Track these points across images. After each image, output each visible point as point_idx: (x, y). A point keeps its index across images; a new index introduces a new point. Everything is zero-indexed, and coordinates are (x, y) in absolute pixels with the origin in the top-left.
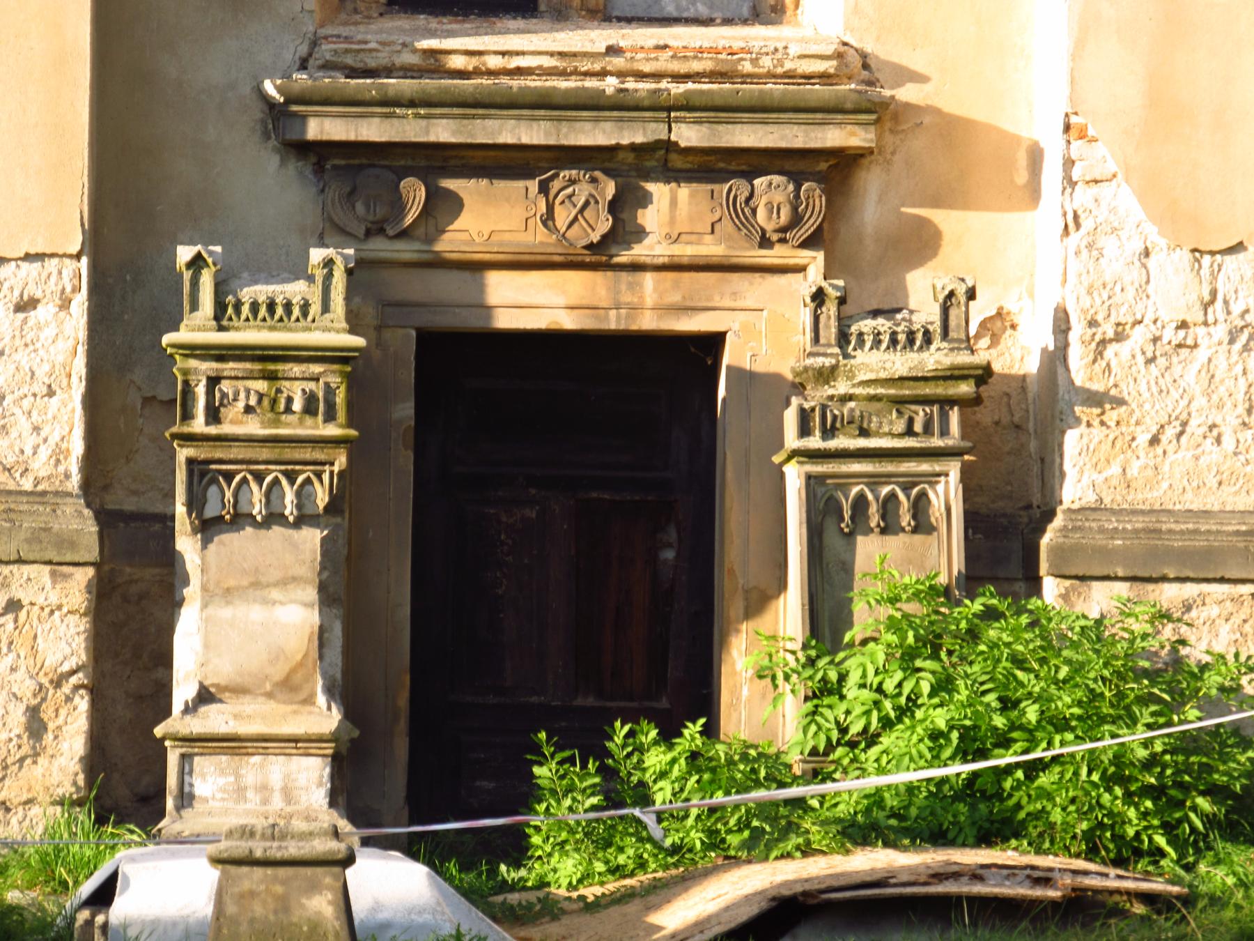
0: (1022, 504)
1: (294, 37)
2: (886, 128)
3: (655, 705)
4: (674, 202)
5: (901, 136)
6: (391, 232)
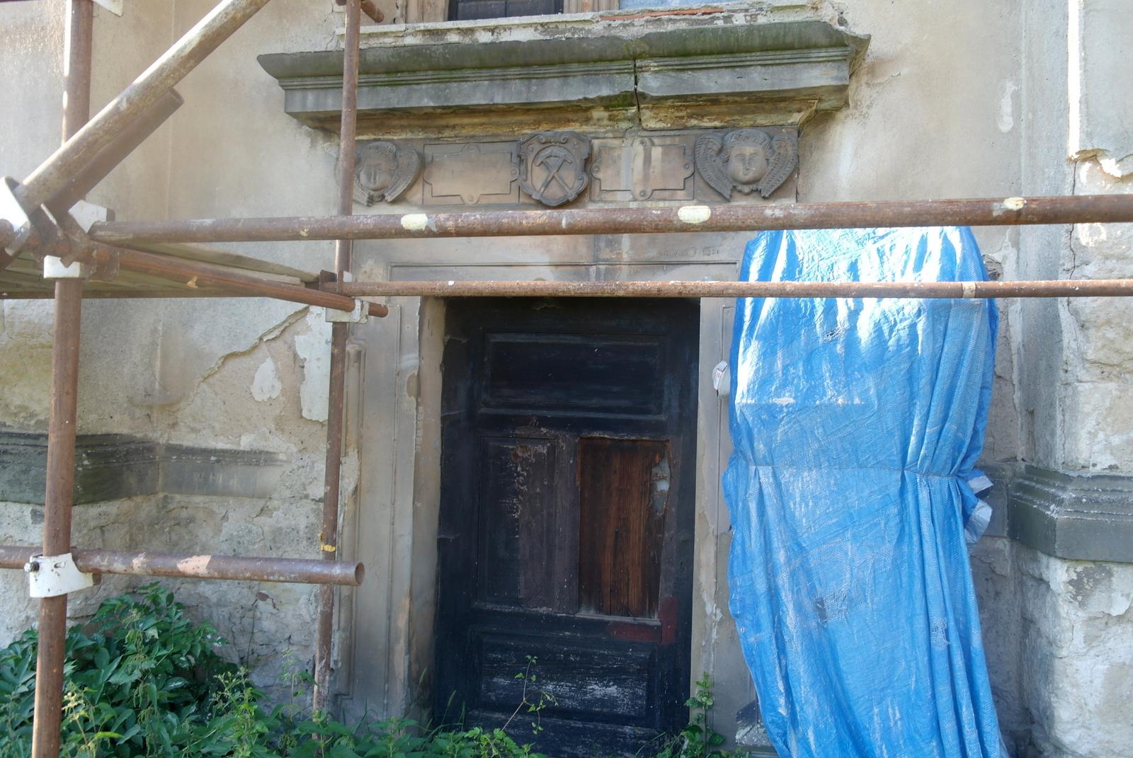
0: (1004, 456)
1: (324, 36)
2: (863, 82)
3: (647, 621)
4: (648, 160)
5: (878, 89)
6: (389, 198)
